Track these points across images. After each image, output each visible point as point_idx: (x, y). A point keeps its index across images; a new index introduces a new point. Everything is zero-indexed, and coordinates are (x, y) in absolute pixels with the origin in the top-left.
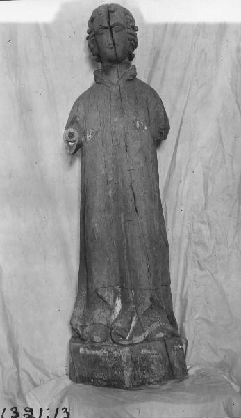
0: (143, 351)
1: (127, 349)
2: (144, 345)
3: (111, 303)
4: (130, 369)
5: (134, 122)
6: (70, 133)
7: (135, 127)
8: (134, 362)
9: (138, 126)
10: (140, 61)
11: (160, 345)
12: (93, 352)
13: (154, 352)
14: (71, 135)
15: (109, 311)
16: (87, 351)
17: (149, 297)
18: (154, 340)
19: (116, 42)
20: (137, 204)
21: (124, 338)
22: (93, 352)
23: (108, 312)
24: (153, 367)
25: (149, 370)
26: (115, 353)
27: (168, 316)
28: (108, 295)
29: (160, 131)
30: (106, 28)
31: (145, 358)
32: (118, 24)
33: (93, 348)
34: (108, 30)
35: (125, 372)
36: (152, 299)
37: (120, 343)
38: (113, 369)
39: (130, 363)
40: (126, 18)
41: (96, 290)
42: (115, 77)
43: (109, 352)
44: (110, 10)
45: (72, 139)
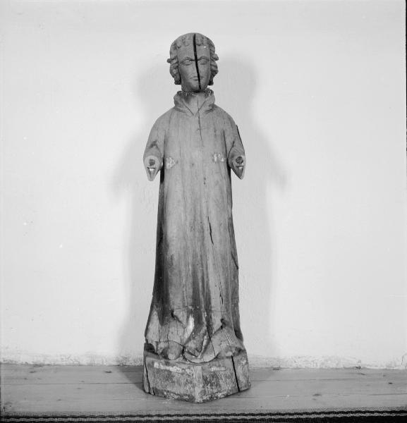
0: (213, 369)
1: (199, 368)
2: (214, 363)
3: (184, 323)
4: (201, 386)
5: (213, 156)
6: (151, 160)
7: (213, 160)
8: (205, 379)
9: (216, 160)
10: (221, 89)
11: (229, 362)
12: (168, 368)
13: (223, 369)
14: (152, 163)
15: (183, 330)
16: (161, 365)
17: (220, 318)
18: (223, 358)
19: (201, 74)
20: (212, 234)
21: (196, 357)
22: (168, 368)
23: (181, 330)
24: (221, 382)
25: (218, 385)
26: (188, 371)
27: (235, 331)
28: (181, 314)
29: (233, 164)
30: (192, 60)
31: (214, 375)
32: (204, 58)
33: (167, 364)
34: (194, 62)
35: (196, 388)
36: (222, 320)
37: (193, 361)
38: (186, 384)
39: (201, 380)
40: (211, 65)
41: (172, 311)
42: (196, 102)
43: (183, 369)
44: (195, 40)
45: (152, 166)
